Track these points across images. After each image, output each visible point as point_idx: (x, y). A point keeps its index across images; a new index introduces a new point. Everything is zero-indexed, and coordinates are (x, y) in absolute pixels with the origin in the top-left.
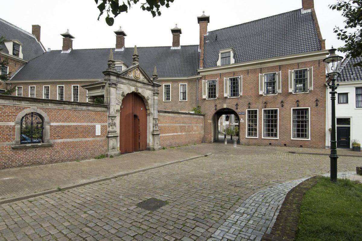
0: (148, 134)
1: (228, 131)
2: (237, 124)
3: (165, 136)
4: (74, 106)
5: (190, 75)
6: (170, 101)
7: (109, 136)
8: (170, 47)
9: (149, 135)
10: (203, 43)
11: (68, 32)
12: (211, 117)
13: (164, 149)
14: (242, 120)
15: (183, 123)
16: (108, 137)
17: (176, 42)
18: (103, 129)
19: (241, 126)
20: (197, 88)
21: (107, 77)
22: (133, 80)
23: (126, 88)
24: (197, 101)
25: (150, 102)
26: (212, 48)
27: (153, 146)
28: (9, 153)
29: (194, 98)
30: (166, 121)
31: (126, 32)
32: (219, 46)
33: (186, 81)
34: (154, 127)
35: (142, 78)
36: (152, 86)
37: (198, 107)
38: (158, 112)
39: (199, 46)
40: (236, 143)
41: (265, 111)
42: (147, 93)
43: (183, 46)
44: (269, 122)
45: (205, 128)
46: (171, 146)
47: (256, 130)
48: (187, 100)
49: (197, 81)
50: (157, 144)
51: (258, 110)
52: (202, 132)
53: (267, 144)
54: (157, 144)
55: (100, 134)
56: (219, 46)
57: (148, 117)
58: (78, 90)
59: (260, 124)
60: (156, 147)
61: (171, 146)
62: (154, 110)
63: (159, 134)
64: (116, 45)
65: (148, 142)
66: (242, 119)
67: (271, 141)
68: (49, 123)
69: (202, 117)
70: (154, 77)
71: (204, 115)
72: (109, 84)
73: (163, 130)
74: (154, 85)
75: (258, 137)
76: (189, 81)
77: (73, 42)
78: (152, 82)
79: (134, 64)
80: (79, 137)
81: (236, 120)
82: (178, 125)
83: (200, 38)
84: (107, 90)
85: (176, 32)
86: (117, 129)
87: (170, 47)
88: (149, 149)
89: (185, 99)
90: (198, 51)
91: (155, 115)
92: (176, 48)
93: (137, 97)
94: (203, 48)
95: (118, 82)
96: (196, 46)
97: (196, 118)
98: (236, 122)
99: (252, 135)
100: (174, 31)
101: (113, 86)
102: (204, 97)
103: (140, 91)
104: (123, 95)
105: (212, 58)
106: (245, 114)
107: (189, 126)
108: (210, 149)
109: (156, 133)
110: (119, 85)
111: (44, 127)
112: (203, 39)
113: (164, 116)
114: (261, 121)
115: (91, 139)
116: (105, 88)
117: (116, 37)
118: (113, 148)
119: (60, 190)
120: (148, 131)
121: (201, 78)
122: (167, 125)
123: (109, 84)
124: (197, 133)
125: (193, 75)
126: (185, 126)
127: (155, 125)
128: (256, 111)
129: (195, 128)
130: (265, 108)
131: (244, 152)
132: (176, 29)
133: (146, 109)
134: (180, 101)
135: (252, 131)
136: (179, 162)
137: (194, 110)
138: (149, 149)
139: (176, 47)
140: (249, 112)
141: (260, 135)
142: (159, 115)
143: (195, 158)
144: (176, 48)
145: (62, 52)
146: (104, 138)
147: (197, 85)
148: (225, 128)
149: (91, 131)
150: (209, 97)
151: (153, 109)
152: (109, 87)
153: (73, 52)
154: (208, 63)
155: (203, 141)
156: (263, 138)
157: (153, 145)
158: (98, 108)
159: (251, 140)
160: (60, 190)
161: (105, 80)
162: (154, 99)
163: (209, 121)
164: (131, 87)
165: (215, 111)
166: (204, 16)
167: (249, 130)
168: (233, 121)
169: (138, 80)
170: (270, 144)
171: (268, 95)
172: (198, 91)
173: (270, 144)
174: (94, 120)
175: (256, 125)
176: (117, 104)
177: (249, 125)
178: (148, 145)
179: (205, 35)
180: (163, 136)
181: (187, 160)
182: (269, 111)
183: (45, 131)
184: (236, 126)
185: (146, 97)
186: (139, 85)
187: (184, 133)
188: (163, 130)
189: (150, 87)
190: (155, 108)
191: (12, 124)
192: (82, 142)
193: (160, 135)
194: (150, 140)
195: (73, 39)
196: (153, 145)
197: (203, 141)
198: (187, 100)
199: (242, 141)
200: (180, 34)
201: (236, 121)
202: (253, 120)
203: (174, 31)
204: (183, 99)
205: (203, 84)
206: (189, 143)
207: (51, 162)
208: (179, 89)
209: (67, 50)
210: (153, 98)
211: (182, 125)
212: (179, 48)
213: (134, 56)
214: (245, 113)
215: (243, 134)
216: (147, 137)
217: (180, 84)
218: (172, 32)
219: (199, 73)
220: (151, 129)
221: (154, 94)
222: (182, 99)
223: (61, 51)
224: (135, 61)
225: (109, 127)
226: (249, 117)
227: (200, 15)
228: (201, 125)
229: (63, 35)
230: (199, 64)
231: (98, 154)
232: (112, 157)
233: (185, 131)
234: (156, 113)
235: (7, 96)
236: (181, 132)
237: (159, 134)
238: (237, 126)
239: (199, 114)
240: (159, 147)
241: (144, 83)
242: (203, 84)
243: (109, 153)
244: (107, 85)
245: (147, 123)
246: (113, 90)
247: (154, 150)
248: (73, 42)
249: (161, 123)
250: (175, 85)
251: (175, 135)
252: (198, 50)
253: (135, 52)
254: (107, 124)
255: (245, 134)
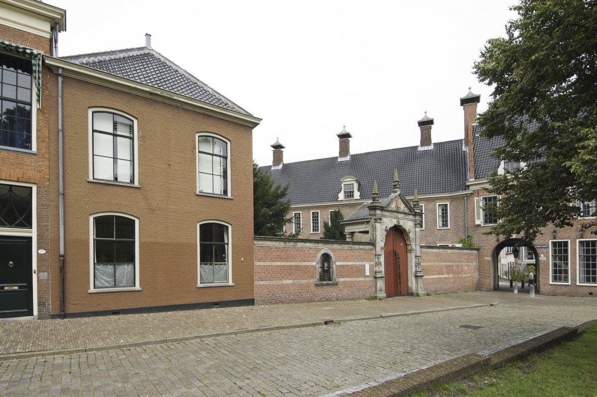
0: (409, 275)
1: (514, 275)
2: (533, 261)
3: (428, 279)
4: (350, 246)
5: (453, 190)
6: (424, 229)
7: (377, 276)
8: (416, 147)
9: (412, 276)
10: (470, 138)
11: (278, 141)
12: (490, 253)
13: (428, 295)
14: (542, 257)
15: (450, 261)
16: (376, 278)
17: (426, 139)
18: (371, 267)
19: (541, 266)
20: (466, 209)
21: (372, 212)
22: (395, 212)
23: (389, 222)
24: (466, 229)
25: (411, 235)
26: (488, 146)
27: (416, 290)
28: (313, 288)
29: (461, 223)
30: (430, 259)
31: (351, 134)
32: (499, 141)
33: (447, 199)
34: (416, 267)
35: (402, 207)
36: (413, 215)
37: (468, 237)
38: (421, 247)
39: (464, 142)
40: (534, 291)
41: (581, 243)
42: (408, 224)
43: (436, 144)
44: (588, 260)
45: (480, 269)
46: (436, 293)
47: (566, 272)
48: (449, 228)
49: (465, 198)
50: (421, 288)
51: (569, 241)
52: (476, 275)
53: (586, 294)
54: (421, 288)
55: (369, 275)
56: (499, 141)
57: (409, 254)
58: (300, 218)
59: (574, 263)
60: (421, 292)
61: (436, 293)
62: (416, 245)
63: (422, 276)
64: (340, 152)
65: (410, 285)
66: (542, 256)
67: (592, 289)
68: (335, 263)
69: (475, 252)
70: (415, 203)
71: (478, 250)
72: (375, 220)
73: (427, 271)
74: (415, 214)
75: (569, 283)
76: (452, 199)
77: (350, 143)
78: (414, 210)
79: (395, 192)
80: (354, 277)
81: (529, 254)
82: (444, 264)
83: (465, 130)
84: (373, 226)
85: (426, 125)
86: (382, 268)
87: (417, 146)
88: (412, 294)
89: (447, 225)
90: (462, 150)
91: (417, 251)
92: (426, 148)
93: (398, 232)
94: (472, 147)
95: (382, 215)
96: (459, 142)
97: (466, 254)
98: (529, 259)
99: (560, 280)
100: (421, 124)
101: (379, 221)
102: (478, 222)
103: (401, 223)
104: (386, 230)
105: (489, 163)
106: (548, 247)
107: (457, 266)
108: (495, 297)
109: (419, 275)
110: (384, 220)
111: (331, 266)
112: (470, 132)
113: (427, 253)
114: (576, 259)
115: (362, 279)
116: (370, 224)
117: (338, 142)
118: (381, 290)
119: (382, 317)
120: (409, 272)
121: (472, 193)
122: (431, 264)
123: (375, 220)
124: (469, 275)
125: (457, 190)
126: (452, 266)
127: (418, 264)
128: (566, 244)
129: (466, 268)
130: (582, 237)
131: (547, 303)
132: (425, 120)
133: (407, 245)
134: (438, 228)
135: (560, 273)
136: (462, 308)
137: (461, 241)
138: (412, 294)
139: (425, 147)
140: (554, 244)
141: (574, 280)
142: (422, 252)
143: (479, 306)
144: (426, 148)
145: (273, 168)
146: (372, 279)
147: (465, 205)
148: (506, 269)
149: (360, 271)
150: (486, 222)
151: (414, 244)
152: (375, 222)
153: (285, 166)
154: (482, 171)
155: (479, 287)
156: (578, 284)
157: (417, 290)
158: (367, 246)
159: (559, 287)
160: (382, 317)
161: (370, 215)
162: (415, 232)
163: (486, 258)
164: (393, 219)
165: (497, 243)
166: (471, 96)
167: (555, 272)
168: (523, 257)
169: (400, 211)
170: (591, 294)
171: (585, 218)
172: (468, 214)
173: (591, 294)
174: (364, 259)
175: (567, 264)
176: (381, 241)
177: (555, 265)
178: (410, 289)
179: (473, 125)
180: (426, 279)
181: (469, 307)
182: (588, 242)
183: (333, 271)
184: (528, 265)
185: (407, 230)
186: (400, 216)
187: (451, 276)
188: (427, 271)
189: (411, 217)
190: (417, 243)
191: (314, 263)
192: (356, 281)
193: (424, 277)
194: (412, 283)
195: (350, 139)
196: (417, 290)
197: (479, 287)
198: (449, 228)
199: (543, 288)
200: (432, 126)
201: (530, 257)
202: (561, 256)
203: (421, 124)
204: (443, 225)
205: (475, 203)
206: (459, 289)
207: (337, 299)
208: (436, 211)
209: (278, 165)
210: (414, 231)
211: (448, 264)
212: (431, 147)
213: (394, 182)
214: (548, 246)
215: (545, 278)
216: (409, 279)
217: (437, 204)
218: (419, 126)
219: (468, 186)
220: (414, 270)
221: (415, 225)
222: (441, 225)
223: (270, 167)
224: (396, 188)
225: (376, 266)
226: (555, 251)
227: (464, 95)
228: (475, 264)
229: (273, 147)
230: (465, 171)
231: (368, 296)
232: (380, 299)
233: (452, 273)
234: (418, 248)
235: (280, 238)
236: (448, 273)
237: (422, 276)
238: (532, 264)
239: (470, 247)
240: (424, 292)
241: (405, 213)
242: (475, 203)
243: (378, 295)
244: (373, 221)
245: (407, 261)
246: (378, 225)
247: (418, 295)
248: (284, 153)
249: (424, 261)
250: (430, 205)
251: (440, 278)
252: (462, 148)
253: (395, 178)
254: (373, 263)
255: (548, 279)
